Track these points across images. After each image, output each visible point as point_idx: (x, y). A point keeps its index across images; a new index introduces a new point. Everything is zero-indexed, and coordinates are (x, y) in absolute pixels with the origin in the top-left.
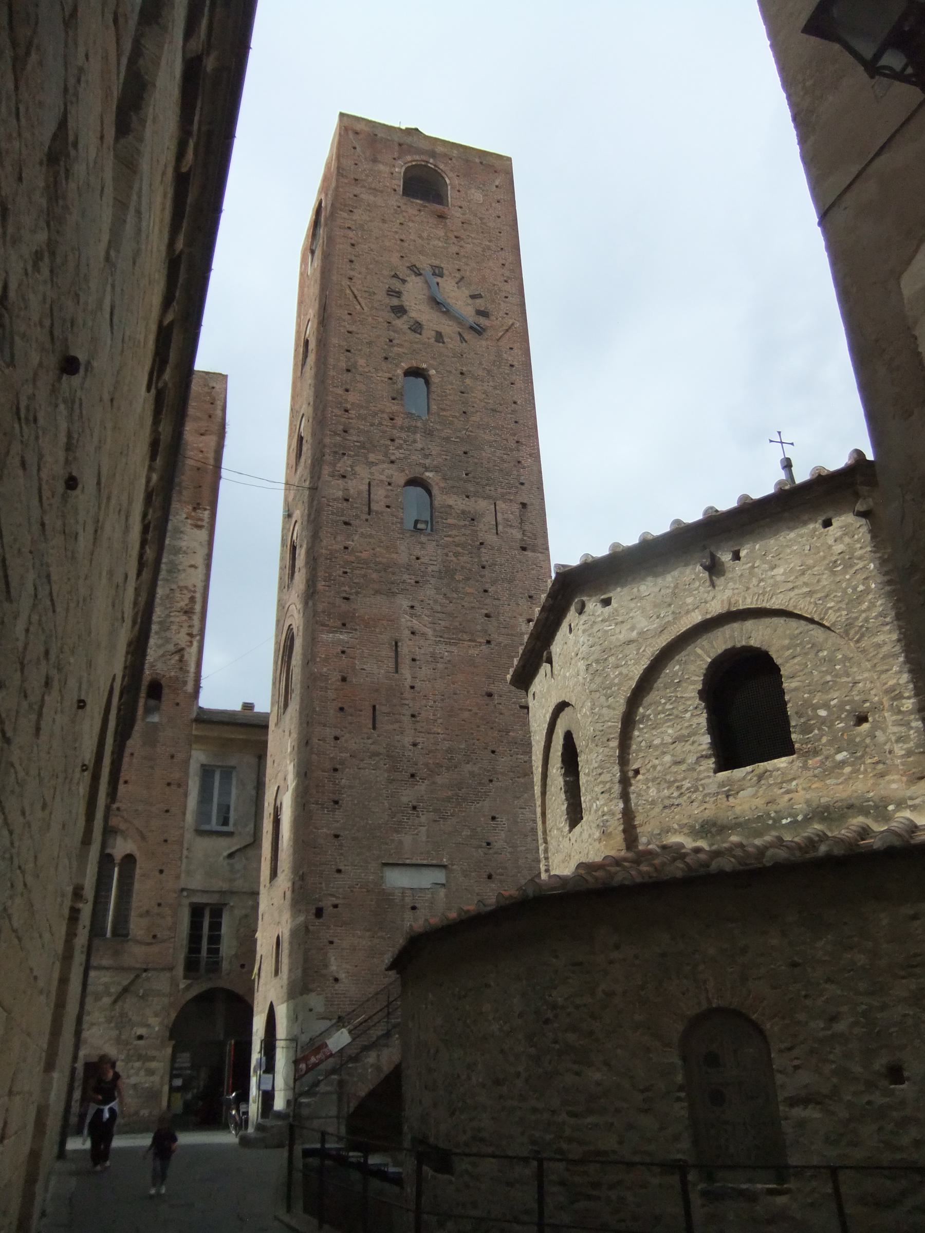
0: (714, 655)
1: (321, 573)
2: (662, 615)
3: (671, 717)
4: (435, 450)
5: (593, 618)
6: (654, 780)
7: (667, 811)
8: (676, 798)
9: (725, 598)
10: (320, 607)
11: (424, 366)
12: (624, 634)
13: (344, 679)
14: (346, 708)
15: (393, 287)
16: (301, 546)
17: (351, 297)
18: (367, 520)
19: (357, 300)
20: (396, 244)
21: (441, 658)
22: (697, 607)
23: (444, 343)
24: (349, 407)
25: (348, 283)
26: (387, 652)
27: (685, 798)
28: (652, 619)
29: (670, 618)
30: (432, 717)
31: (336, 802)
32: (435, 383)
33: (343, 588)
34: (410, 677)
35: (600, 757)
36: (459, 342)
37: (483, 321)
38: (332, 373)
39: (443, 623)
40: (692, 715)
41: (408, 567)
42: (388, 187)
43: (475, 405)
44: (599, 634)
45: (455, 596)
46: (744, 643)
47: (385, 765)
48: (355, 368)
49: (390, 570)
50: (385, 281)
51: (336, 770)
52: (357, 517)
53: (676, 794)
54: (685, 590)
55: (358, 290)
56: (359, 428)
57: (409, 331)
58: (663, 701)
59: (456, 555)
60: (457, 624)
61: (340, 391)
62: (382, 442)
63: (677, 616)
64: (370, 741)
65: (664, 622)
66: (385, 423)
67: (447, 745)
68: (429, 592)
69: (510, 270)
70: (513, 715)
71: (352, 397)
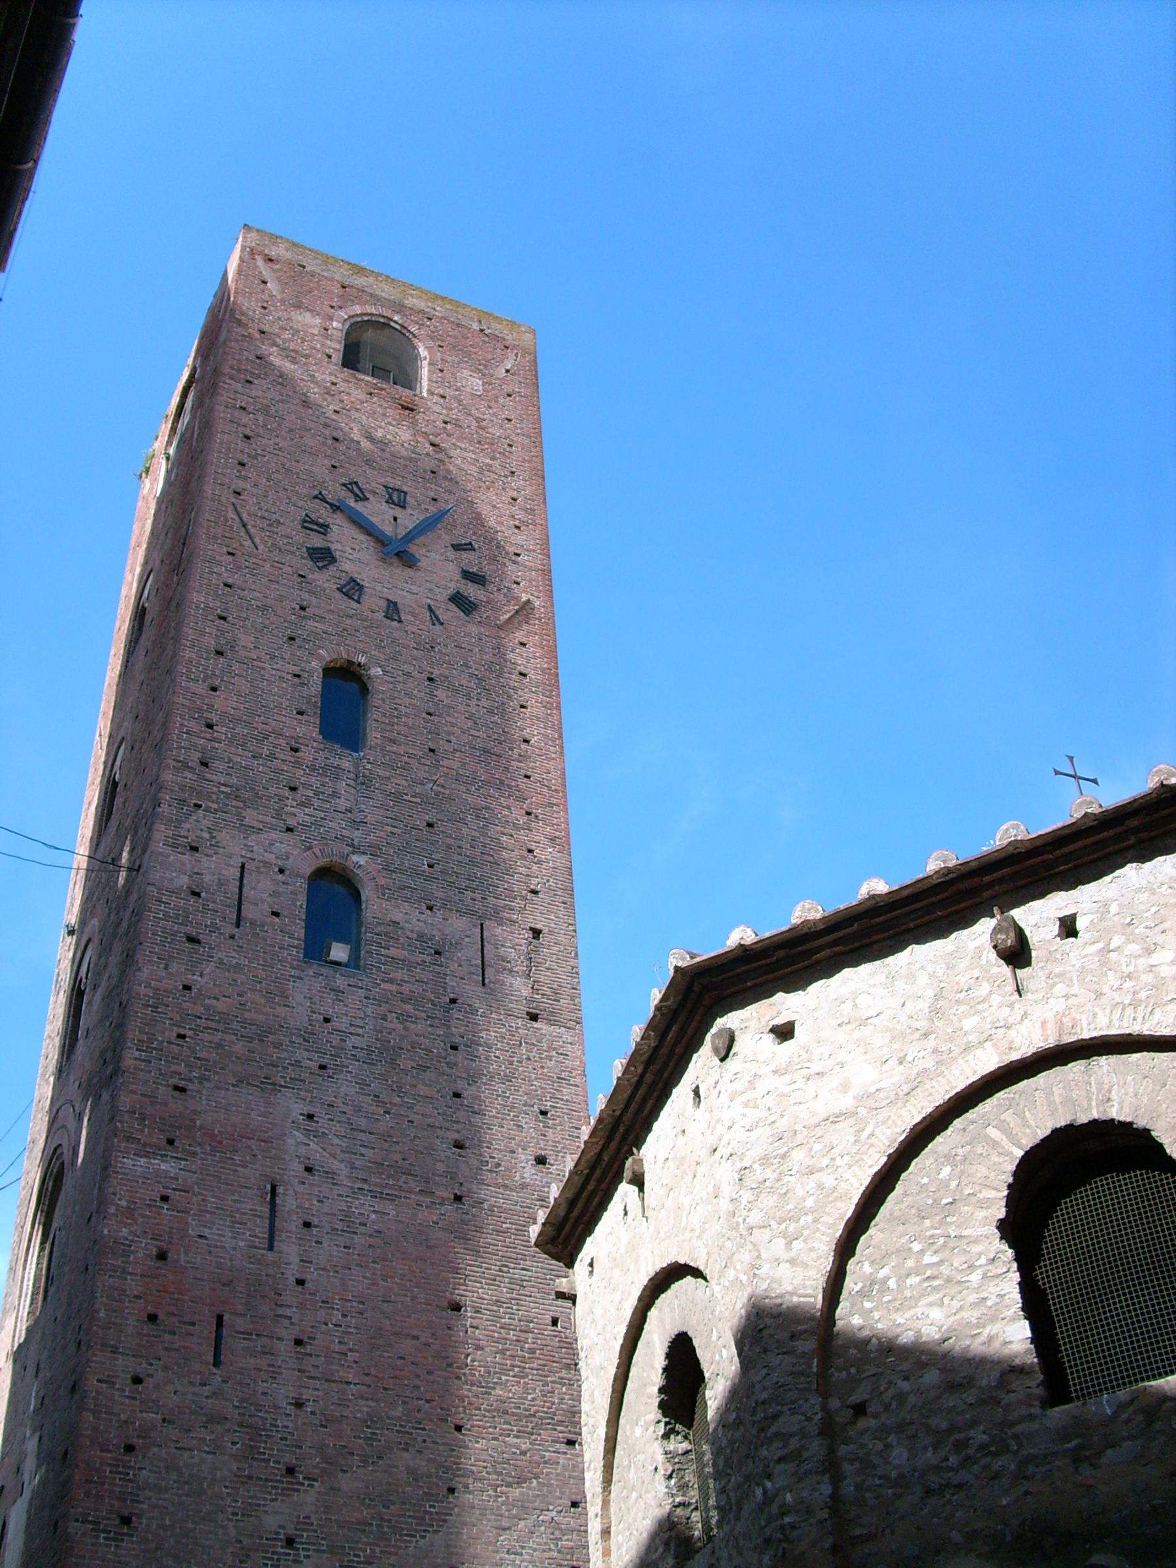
0: (1029, 1142)
1: (133, 1034)
2: (909, 1058)
3: (936, 1283)
4: (372, 813)
5: (754, 1068)
6: (900, 1428)
7: (933, 1501)
8: (955, 1470)
9: (1050, 1016)
10: (126, 1101)
11: (362, 659)
12: (828, 1100)
13: (162, 1256)
14: (161, 1316)
15: (313, 516)
16: (95, 987)
17: (237, 525)
18: (232, 937)
19: (248, 532)
20: (324, 444)
21: (360, 1224)
22: (989, 1038)
23: (400, 621)
24: (215, 719)
25: (233, 500)
26: (253, 1205)
27: (976, 1469)
28: (886, 1067)
29: (930, 1064)
30: (337, 1348)
31: (126, 1521)
32: (378, 691)
33: (174, 1068)
34: (298, 1260)
35: (774, 1377)
36: (429, 624)
37: (472, 591)
38: (187, 654)
39: (368, 1153)
40: (985, 1276)
41: (307, 1036)
42: (318, 350)
43: (454, 740)
44: (769, 1101)
45: (397, 1100)
46: (1095, 1115)
47: (234, 1443)
48: (232, 648)
49: (271, 1038)
50: (301, 504)
51: (130, 1449)
52: (214, 928)
53: (953, 1460)
54: (958, 1002)
55: (249, 514)
56: (230, 760)
57: (338, 595)
58: (916, 1246)
59: (403, 1018)
60: (398, 1157)
61: (201, 689)
62: (273, 790)
63: (943, 1060)
64: (207, 1390)
65: (914, 1073)
66: (282, 756)
67: (363, 1408)
68: (345, 1088)
69: (526, 510)
70: (502, 1352)
71: (219, 701)
